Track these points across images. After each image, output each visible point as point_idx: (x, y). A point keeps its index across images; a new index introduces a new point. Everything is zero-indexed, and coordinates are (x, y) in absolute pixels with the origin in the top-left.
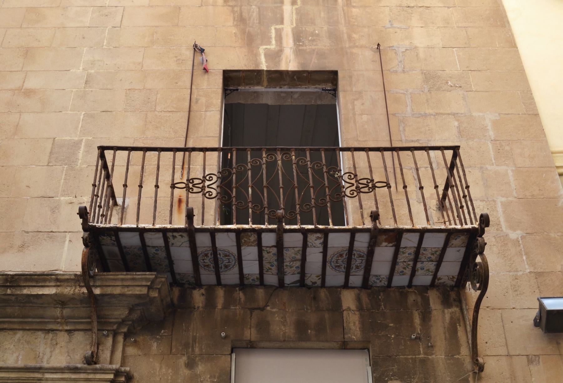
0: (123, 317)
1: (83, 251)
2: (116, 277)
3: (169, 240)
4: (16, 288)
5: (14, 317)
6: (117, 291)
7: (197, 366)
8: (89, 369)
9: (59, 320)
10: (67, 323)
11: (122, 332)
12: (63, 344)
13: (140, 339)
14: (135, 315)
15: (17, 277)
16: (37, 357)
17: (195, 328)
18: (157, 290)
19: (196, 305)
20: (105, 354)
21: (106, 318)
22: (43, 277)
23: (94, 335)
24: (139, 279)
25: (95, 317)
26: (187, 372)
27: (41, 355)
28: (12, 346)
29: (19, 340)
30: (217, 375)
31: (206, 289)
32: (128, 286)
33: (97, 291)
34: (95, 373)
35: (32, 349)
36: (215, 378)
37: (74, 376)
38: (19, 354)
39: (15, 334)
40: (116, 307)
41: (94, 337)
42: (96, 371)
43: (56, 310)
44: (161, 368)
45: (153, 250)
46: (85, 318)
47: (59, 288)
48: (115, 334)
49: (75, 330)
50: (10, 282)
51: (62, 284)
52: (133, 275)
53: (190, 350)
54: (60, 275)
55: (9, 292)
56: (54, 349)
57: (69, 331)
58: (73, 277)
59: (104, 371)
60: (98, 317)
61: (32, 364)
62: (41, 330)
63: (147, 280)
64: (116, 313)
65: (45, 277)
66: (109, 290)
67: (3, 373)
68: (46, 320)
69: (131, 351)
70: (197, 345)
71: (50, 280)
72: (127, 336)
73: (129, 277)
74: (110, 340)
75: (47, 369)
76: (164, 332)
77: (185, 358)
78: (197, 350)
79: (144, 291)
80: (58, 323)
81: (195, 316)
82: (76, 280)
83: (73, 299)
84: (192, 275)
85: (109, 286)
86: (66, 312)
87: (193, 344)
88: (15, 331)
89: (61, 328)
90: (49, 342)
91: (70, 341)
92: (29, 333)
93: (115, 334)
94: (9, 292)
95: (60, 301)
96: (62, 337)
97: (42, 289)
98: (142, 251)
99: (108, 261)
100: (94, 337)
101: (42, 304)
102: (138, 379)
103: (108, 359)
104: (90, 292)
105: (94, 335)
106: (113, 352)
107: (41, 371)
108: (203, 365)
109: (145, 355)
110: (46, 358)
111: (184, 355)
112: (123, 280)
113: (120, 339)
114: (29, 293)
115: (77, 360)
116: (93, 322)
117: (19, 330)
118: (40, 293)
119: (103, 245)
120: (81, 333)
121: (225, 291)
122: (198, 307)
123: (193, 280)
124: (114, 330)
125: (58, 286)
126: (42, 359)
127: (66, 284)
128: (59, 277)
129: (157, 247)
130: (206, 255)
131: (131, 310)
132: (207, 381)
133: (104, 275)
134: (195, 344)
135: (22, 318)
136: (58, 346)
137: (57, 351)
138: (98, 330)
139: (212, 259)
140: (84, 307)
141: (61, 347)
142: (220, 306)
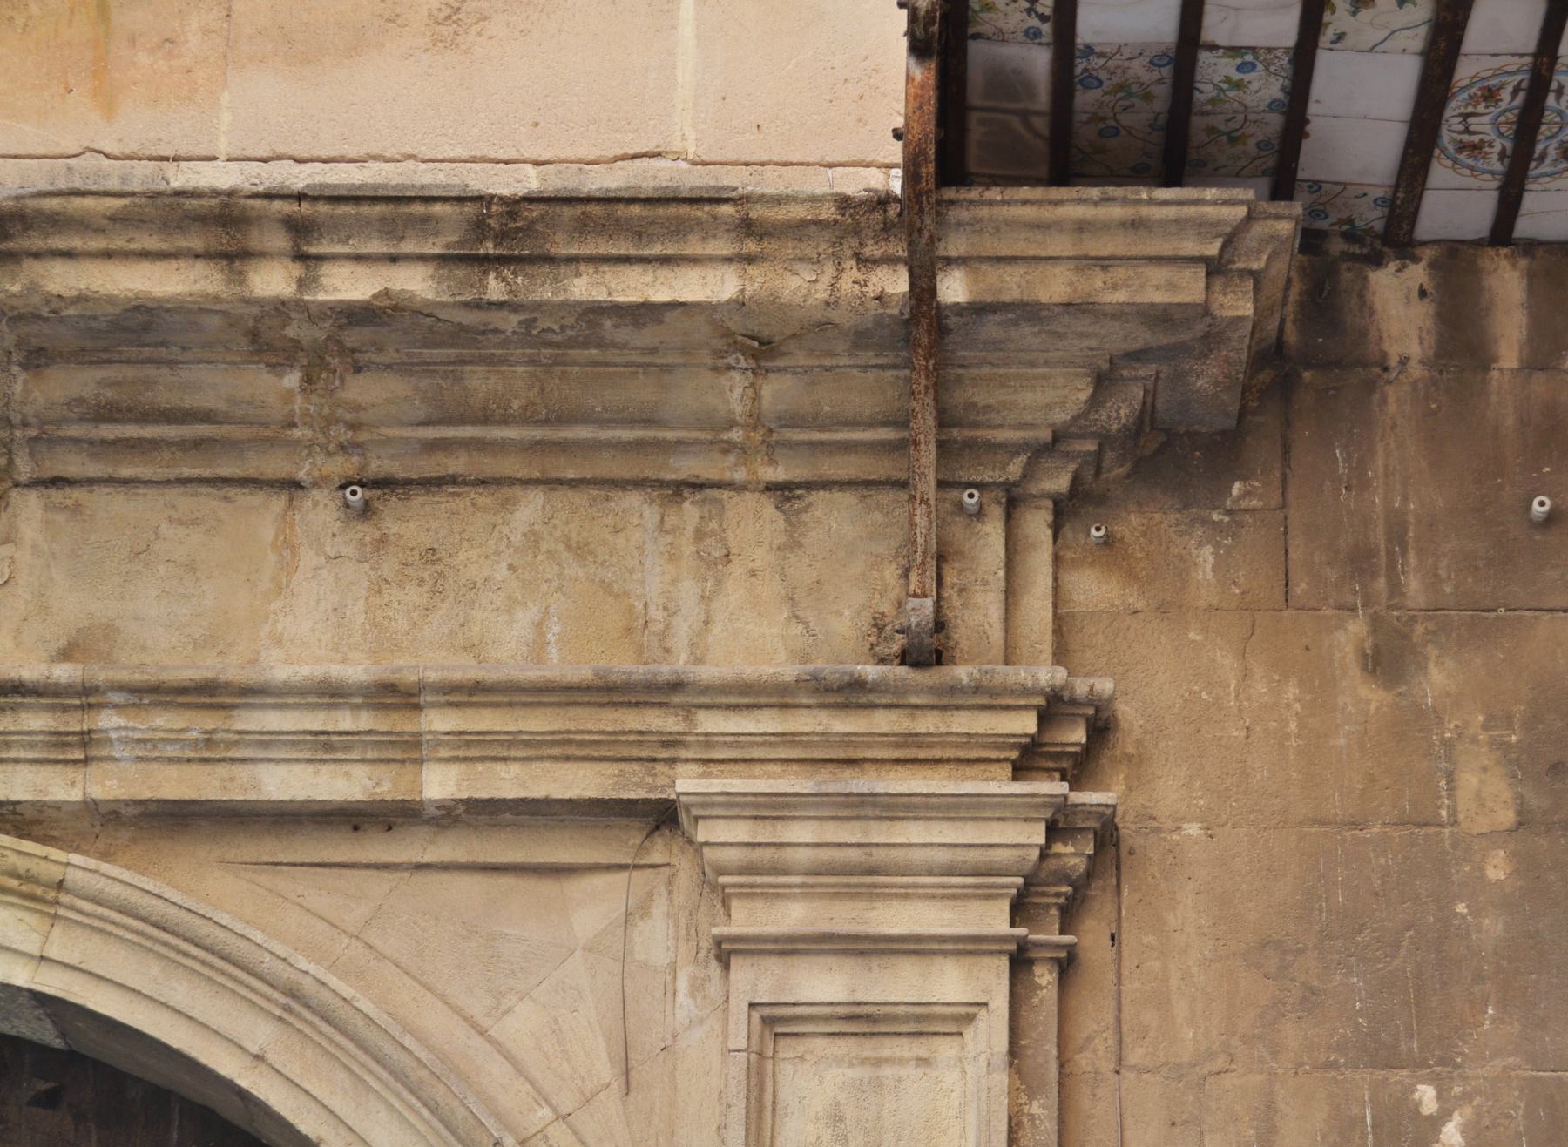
0: (1060, 417)
1: (909, 79)
2: (1047, 213)
3: (1327, 17)
4: (530, 269)
5: (505, 421)
6: (1055, 286)
7: (1423, 668)
8: (918, 690)
9: (736, 435)
10: (771, 450)
11: (1045, 495)
12: (761, 557)
13: (1130, 525)
14: (1120, 412)
15: (536, 211)
16: (634, 628)
17: (1395, 471)
18: (1250, 284)
19: (1394, 352)
20: (979, 614)
21: (975, 425)
22: (672, 210)
23: (921, 510)
24: (1164, 224)
25: (926, 421)
26: (1373, 696)
27: (656, 614)
28: (502, 572)
29: (533, 539)
30: (1519, 710)
31: (1433, 265)
32: (1105, 263)
33: (953, 289)
34: (945, 708)
35: (606, 587)
36: (1509, 725)
37: (842, 724)
38: (546, 612)
39: (507, 505)
40: (1033, 364)
41: (921, 521)
42: (950, 699)
43: (723, 381)
44: (1246, 674)
45: (1226, 67)
46: (872, 424)
47: (753, 270)
48: (1013, 502)
49: (809, 486)
50: (501, 237)
51: (770, 246)
52: (1139, 202)
53: (1381, 583)
54: (762, 199)
55: (495, 288)
56: (719, 582)
57: (782, 491)
58: (828, 212)
59: (988, 697)
60: (944, 420)
61: (625, 665)
62: (639, 484)
63: (1203, 228)
64: (1027, 397)
65: (685, 210)
66: (1011, 284)
67: (486, 712)
68: (670, 435)
69: (1092, 588)
70: (1412, 559)
71: (707, 230)
72: (1064, 511)
73: (1117, 212)
74: (993, 532)
75: (707, 689)
76: (1246, 494)
77: (1357, 628)
78: (1414, 586)
79: (1190, 287)
80: (728, 448)
81: (1392, 408)
82: (854, 223)
83: (823, 326)
84: (1380, 193)
85: (1012, 260)
86: (778, 391)
87: (1390, 554)
88: (506, 491)
89: (740, 475)
90: (688, 549)
91: (792, 544)
92: (579, 498)
93: (1013, 502)
94: (495, 288)
95: (755, 341)
96: (752, 524)
97: (664, 272)
98: (1166, 72)
99: (974, 117)
100: (921, 521)
101: (654, 351)
102: (1137, 734)
103: (997, 635)
104: (923, 290)
105: (921, 510)
106: (1011, 594)
107: (677, 699)
108: (1450, 664)
109: (1162, 609)
110: (683, 630)
111: (1353, 609)
112: (1082, 227)
113: (1037, 524)
114: (601, 296)
115: (841, 634)
116: (916, 444)
117: (527, 483)
118: (660, 296)
119: (977, 36)
120: (847, 498)
121: (1531, 276)
122: (1404, 361)
123: (1372, 217)
124: (1008, 487)
125: (750, 259)
126: (663, 635)
127: (789, 248)
128: (758, 212)
129: (1253, 49)
130: (1490, 95)
131: (1104, 382)
132: (1474, 740)
133: (991, 203)
134: (1404, 553)
135: (546, 422)
136: (737, 569)
137: (735, 592)
138: (942, 484)
139: (1511, 116)
140: (865, 368)
141: (753, 573)
142: (1509, 354)
